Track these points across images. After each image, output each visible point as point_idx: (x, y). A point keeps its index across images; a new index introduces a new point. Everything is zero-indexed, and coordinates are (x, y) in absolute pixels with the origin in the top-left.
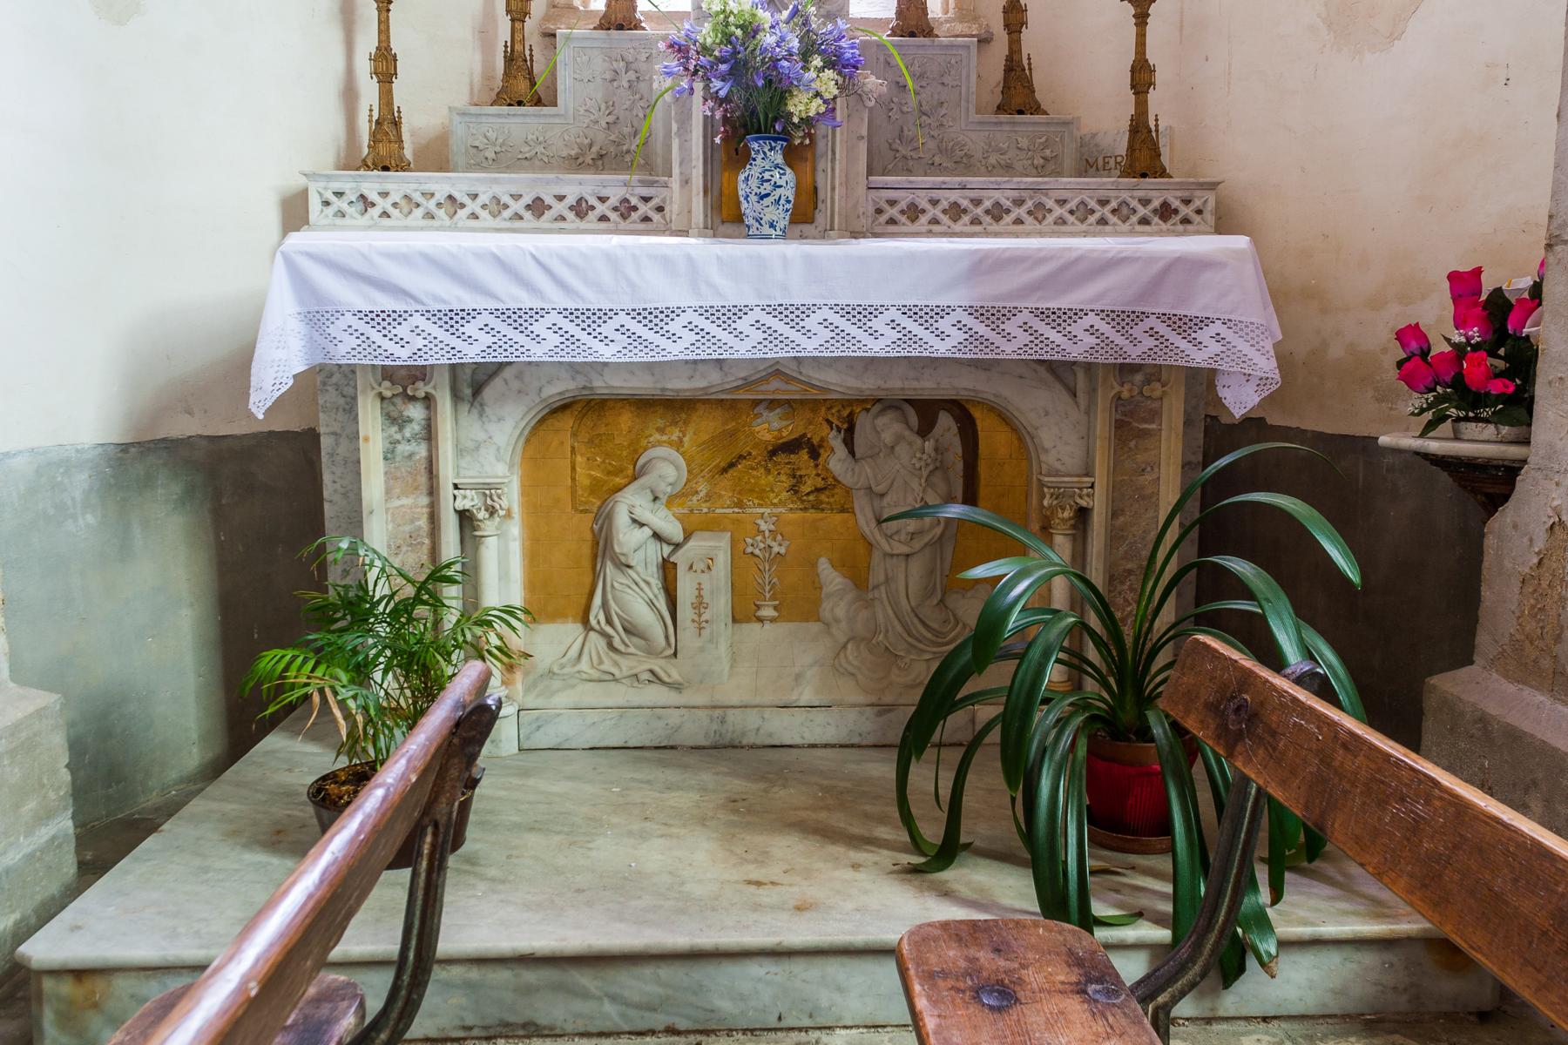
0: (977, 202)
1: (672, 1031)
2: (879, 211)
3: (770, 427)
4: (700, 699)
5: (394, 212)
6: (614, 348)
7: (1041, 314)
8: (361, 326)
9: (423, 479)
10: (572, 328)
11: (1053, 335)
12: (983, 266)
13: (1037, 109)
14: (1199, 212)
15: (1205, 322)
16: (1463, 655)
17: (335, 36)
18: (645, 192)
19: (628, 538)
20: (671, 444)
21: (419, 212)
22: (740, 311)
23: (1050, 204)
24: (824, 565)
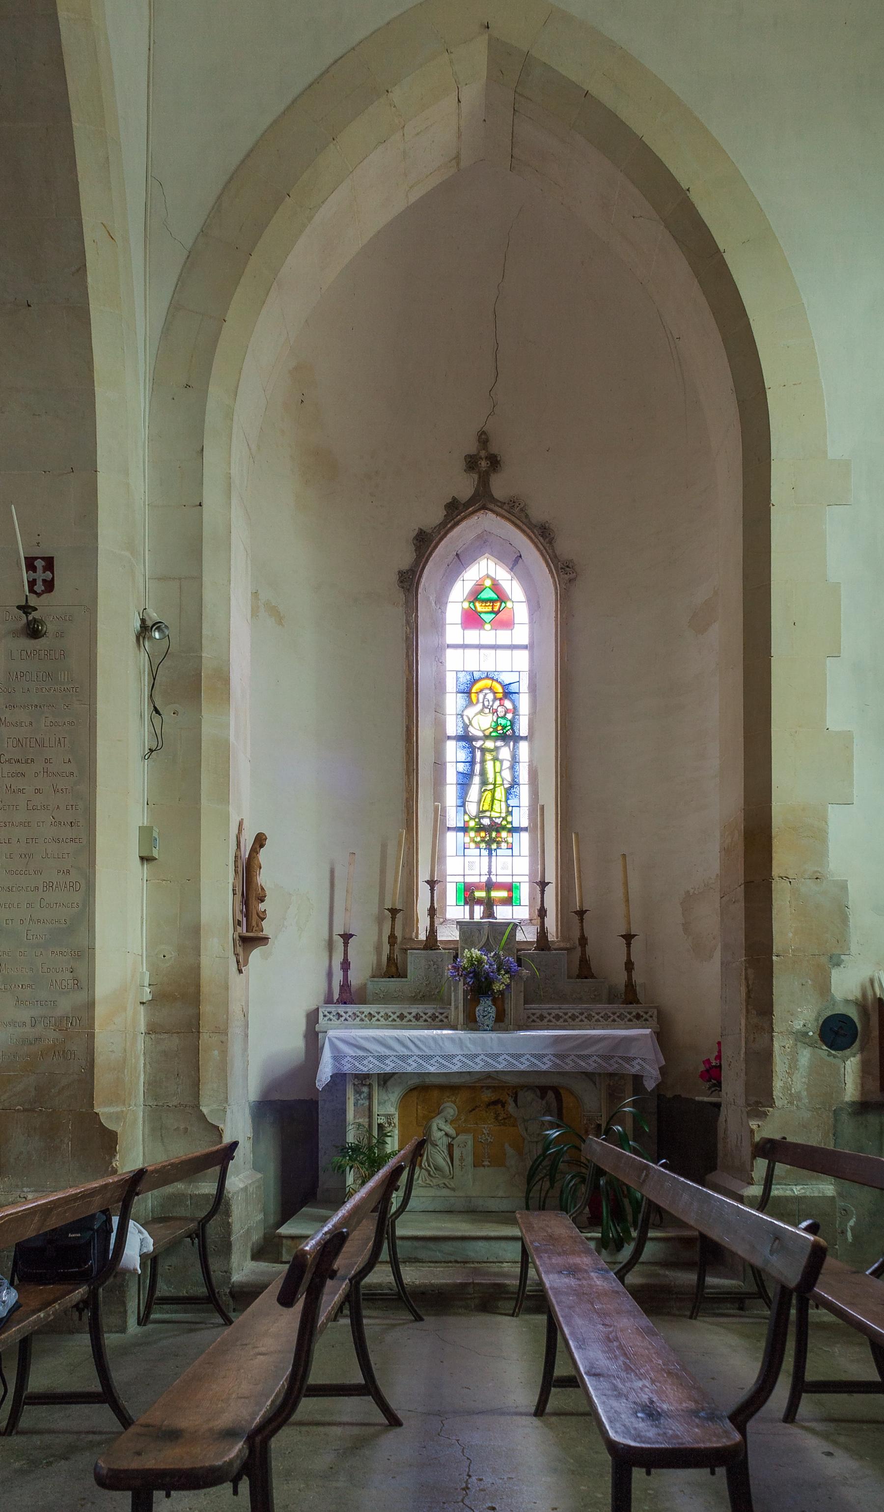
0: (566, 1014)
1: (456, 1262)
2: (529, 1017)
3: (487, 1096)
4: (461, 1194)
5: (349, 1019)
6: (434, 1068)
7: (578, 1056)
8: (352, 1061)
9: (367, 1113)
10: (421, 1061)
11: (583, 1064)
12: (557, 1040)
13: (592, 976)
14: (651, 1017)
15: (635, 1058)
16: (714, 1168)
17: (326, 955)
18: (441, 1011)
19: (437, 1135)
20: (452, 1102)
21: (358, 1019)
22: (477, 1056)
23: (593, 1014)
24: (507, 1145)
